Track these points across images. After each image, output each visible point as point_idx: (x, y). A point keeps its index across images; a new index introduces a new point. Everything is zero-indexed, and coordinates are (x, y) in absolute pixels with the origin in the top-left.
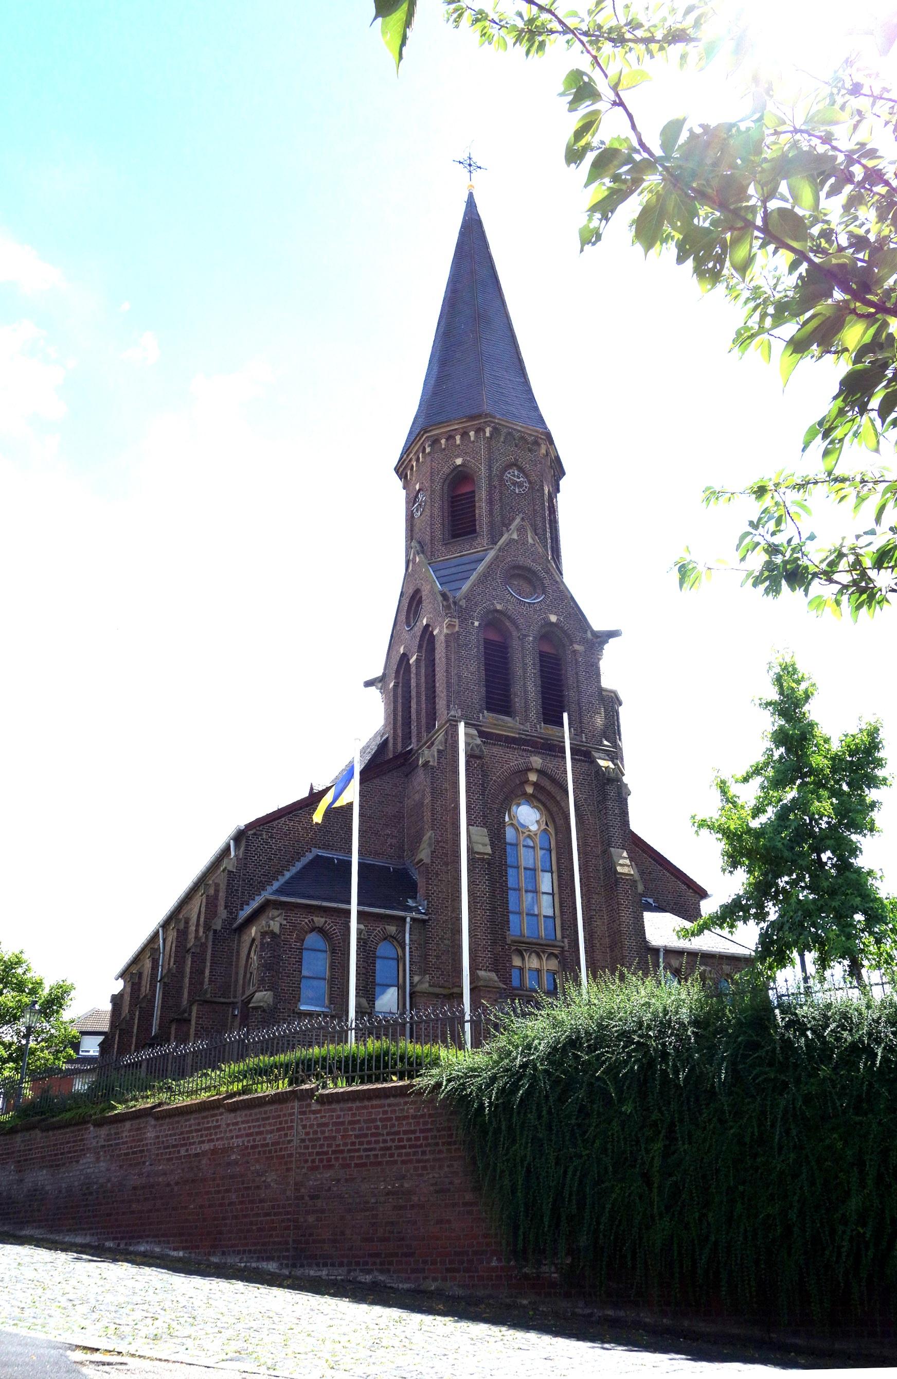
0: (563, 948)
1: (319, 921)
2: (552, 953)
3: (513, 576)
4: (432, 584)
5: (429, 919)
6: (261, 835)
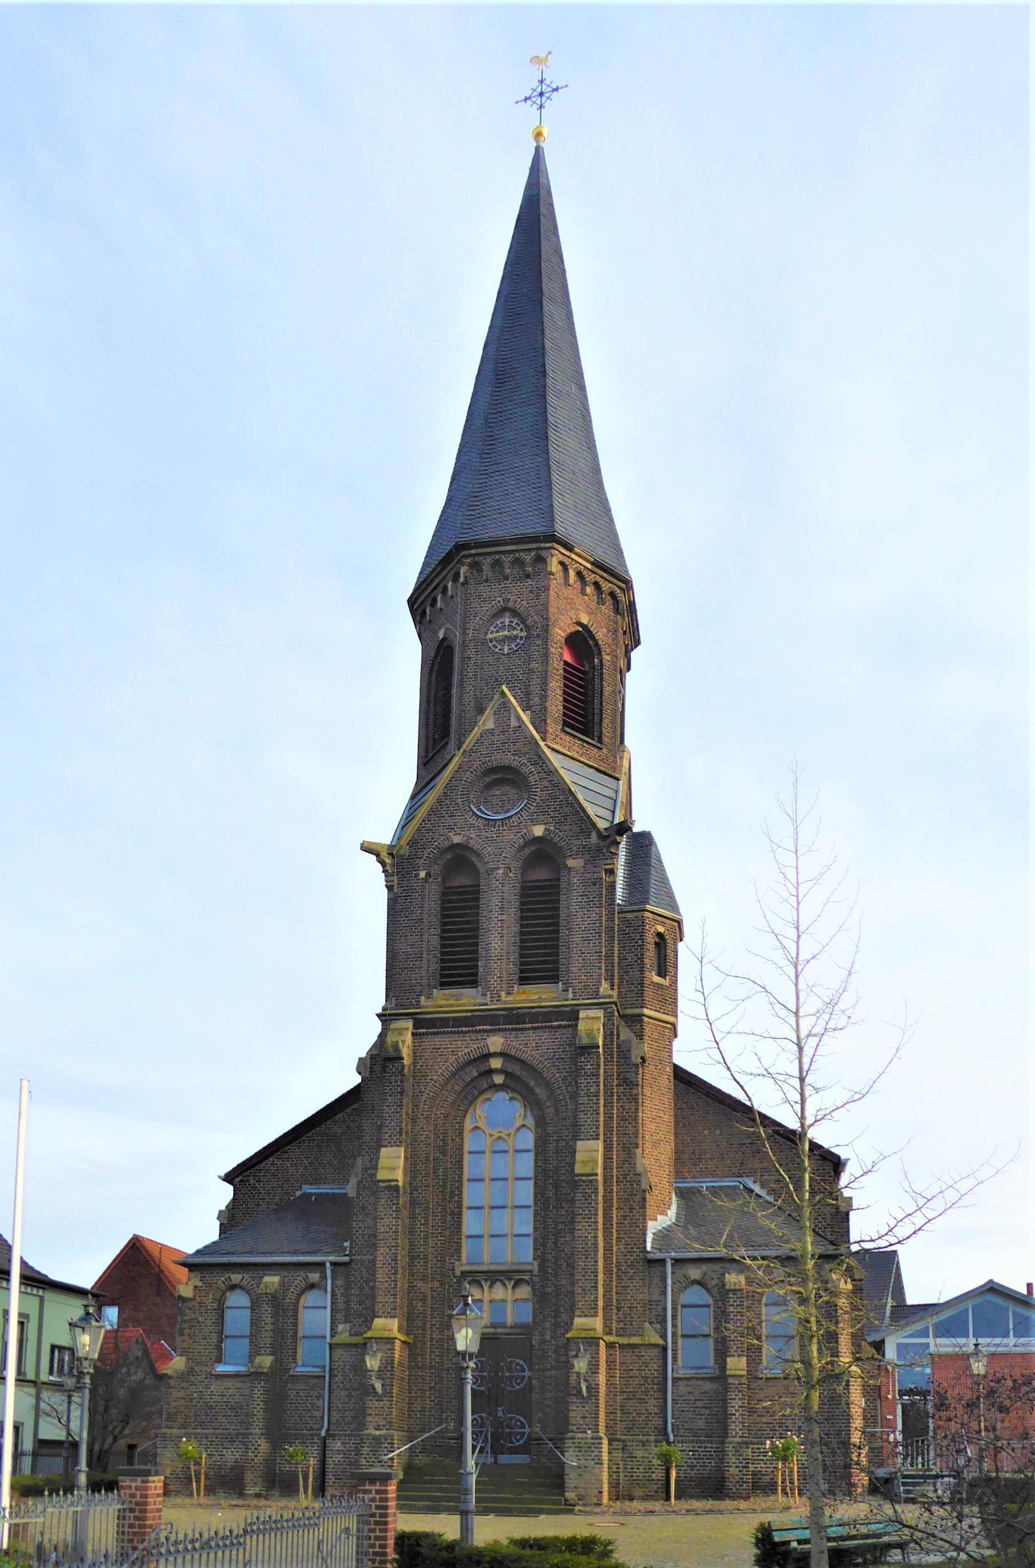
0: (531, 1271)
1: (236, 1278)
2: (520, 1280)
3: (489, 786)
4: (568, 763)
5: (351, 1261)
6: (248, 1181)
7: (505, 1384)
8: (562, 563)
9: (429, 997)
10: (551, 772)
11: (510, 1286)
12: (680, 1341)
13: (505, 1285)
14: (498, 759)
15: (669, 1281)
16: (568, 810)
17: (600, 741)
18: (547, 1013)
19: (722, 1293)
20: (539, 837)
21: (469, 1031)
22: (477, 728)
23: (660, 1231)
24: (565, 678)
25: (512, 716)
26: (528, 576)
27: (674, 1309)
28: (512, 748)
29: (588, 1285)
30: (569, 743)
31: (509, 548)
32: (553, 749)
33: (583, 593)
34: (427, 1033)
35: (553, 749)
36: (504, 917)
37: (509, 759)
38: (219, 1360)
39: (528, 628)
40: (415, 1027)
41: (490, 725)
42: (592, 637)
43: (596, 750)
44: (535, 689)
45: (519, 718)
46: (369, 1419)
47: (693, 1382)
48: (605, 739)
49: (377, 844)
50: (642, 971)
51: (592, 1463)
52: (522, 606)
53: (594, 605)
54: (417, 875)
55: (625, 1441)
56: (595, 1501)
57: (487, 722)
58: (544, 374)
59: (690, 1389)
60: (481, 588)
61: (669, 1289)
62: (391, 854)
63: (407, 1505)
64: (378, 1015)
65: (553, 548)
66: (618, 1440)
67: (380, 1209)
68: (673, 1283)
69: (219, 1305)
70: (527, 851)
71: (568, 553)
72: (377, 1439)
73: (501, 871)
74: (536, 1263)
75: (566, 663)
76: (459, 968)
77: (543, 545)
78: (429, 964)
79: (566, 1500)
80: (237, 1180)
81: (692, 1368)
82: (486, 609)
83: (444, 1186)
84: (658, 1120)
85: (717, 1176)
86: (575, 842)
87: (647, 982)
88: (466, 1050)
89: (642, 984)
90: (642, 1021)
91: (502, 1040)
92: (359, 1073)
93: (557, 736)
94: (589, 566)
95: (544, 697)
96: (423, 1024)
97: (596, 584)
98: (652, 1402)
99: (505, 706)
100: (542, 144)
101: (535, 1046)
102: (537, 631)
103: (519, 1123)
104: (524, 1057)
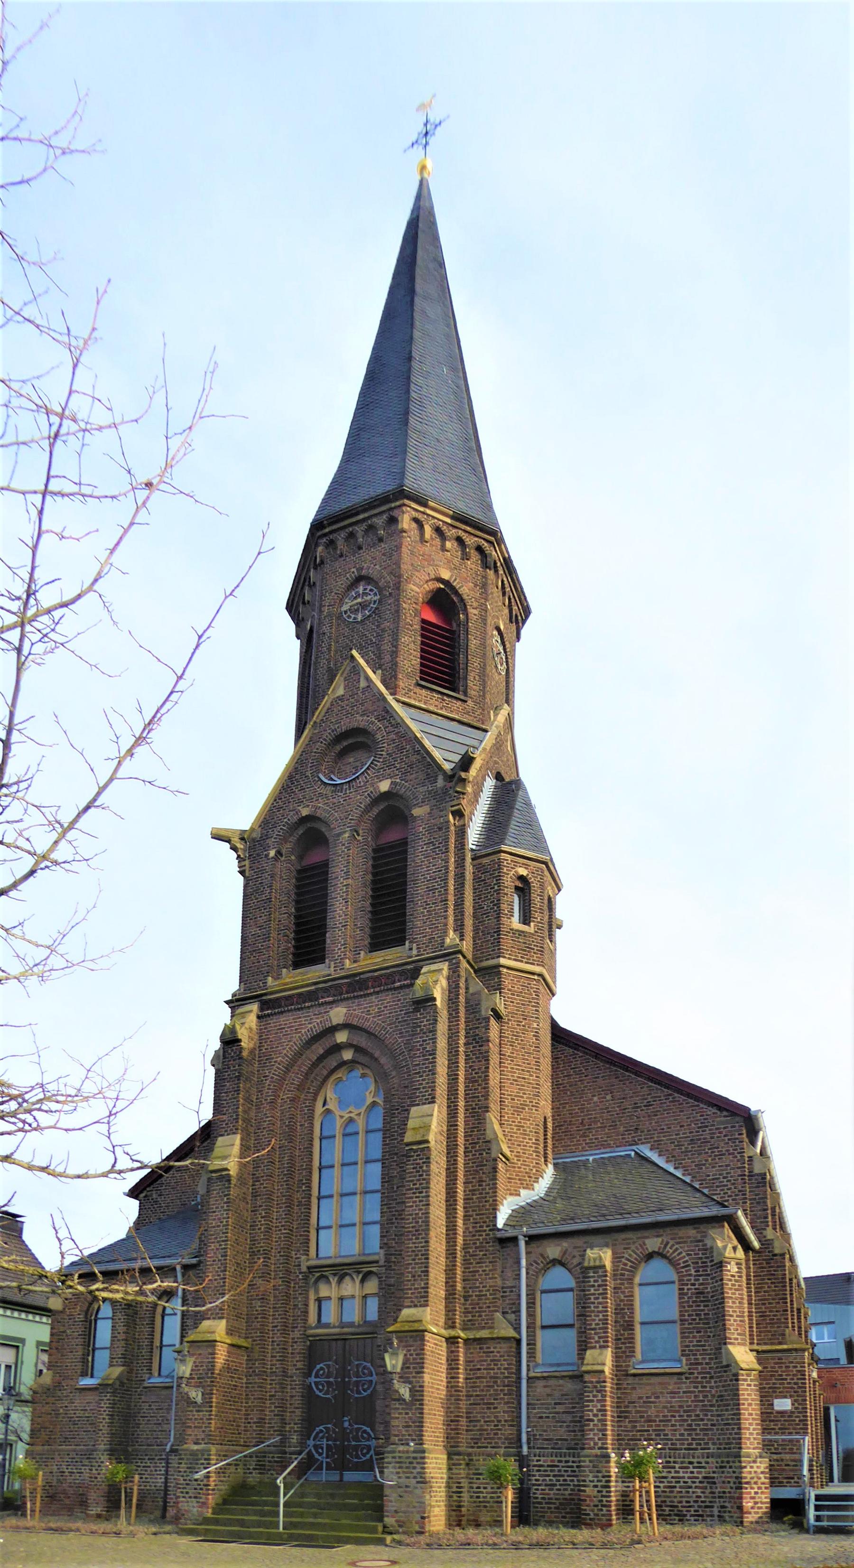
2: (370, 1273)
6: (151, 1195)
7: (352, 1391)
8: (416, 520)
9: (278, 977)
10: (398, 725)
11: (358, 1281)
12: (539, 1333)
13: (353, 1279)
14: (346, 724)
15: (524, 1262)
16: (414, 758)
17: (465, 693)
18: (391, 974)
19: (585, 1273)
20: (385, 793)
21: (312, 1006)
22: (326, 697)
23: (522, 1207)
24: (422, 636)
25: (362, 679)
26: (381, 540)
27: (531, 1295)
28: (361, 709)
29: (418, 1270)
30: (430, 699)
31: (361, 517)
32: (404, 703)
33: (444, 549)
34: (272, 1014)
35: (404, 703)
36: (350, 881)
37: (360, 721)
38: (84, 1374)
39: (380, 590)
40: (261, 1009)
41: (341, 692)
42: (453, 588)
43: (459, 703)
44: (386, 647)
45: (368, 678)
46: (189, 1432)
47: (552, 1382)
48: (472, 693)
49: (226, 830)
50: (498, 918)
51: (414, 1481)
52: (373, 570)
53: (457, 561)
54: (267, 856)
55: (469, 1455)
56: (417, 1528)
57: (339, 689)
58: (410, 358)
59: (548, 1390)
60: (337, 564)
61: (524, 1272)
62: (242, 839)
63: (278, 1528)
64: (227, 1002)
65: (405, 505)
66: (459, 1454)
67: (212, 1201)
68: (529, 1265)
69: (86, 1317)
70: (376, 811)
71: (421, 509)
72: (194, 1453)
73: (347, 835)
74: (382, 1252)
75: (424, 621)
76: (309, 945)
77: (393, 505)
78: (281, 941)
79: (385, 1527)
80: (142, 1195)
81: (552, 1365)
82: (342, 583)
83: (290, 1175)
84: (522, 1082)
85: (609, 1146)
86: (421, 789)
87: (504, 929)
88: (310, 1026)
89: (498, 932)
90: (499, 973)
91: (345, 1010)
92: (213, 1065)
93: (410, 690)
94: (449, 520)
95: (395, 653)
96: (271, 1006)
97: (459, 540)
98: (502, 1407)
99: (356, 670)
100: (426, 175)
101: (376, 1011)
102: (391, 590)
103: (369, 1100)
104: (366, 1025)
